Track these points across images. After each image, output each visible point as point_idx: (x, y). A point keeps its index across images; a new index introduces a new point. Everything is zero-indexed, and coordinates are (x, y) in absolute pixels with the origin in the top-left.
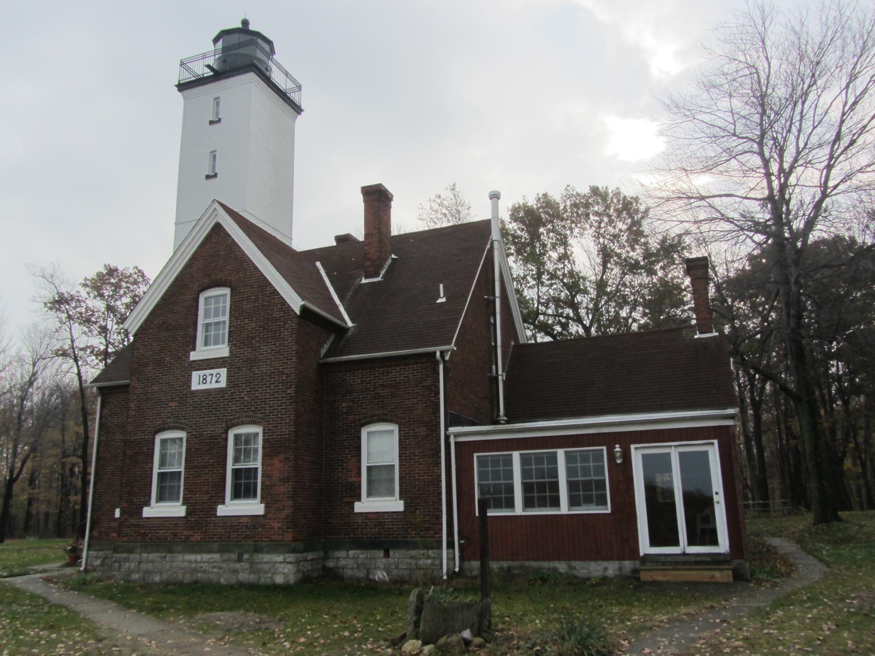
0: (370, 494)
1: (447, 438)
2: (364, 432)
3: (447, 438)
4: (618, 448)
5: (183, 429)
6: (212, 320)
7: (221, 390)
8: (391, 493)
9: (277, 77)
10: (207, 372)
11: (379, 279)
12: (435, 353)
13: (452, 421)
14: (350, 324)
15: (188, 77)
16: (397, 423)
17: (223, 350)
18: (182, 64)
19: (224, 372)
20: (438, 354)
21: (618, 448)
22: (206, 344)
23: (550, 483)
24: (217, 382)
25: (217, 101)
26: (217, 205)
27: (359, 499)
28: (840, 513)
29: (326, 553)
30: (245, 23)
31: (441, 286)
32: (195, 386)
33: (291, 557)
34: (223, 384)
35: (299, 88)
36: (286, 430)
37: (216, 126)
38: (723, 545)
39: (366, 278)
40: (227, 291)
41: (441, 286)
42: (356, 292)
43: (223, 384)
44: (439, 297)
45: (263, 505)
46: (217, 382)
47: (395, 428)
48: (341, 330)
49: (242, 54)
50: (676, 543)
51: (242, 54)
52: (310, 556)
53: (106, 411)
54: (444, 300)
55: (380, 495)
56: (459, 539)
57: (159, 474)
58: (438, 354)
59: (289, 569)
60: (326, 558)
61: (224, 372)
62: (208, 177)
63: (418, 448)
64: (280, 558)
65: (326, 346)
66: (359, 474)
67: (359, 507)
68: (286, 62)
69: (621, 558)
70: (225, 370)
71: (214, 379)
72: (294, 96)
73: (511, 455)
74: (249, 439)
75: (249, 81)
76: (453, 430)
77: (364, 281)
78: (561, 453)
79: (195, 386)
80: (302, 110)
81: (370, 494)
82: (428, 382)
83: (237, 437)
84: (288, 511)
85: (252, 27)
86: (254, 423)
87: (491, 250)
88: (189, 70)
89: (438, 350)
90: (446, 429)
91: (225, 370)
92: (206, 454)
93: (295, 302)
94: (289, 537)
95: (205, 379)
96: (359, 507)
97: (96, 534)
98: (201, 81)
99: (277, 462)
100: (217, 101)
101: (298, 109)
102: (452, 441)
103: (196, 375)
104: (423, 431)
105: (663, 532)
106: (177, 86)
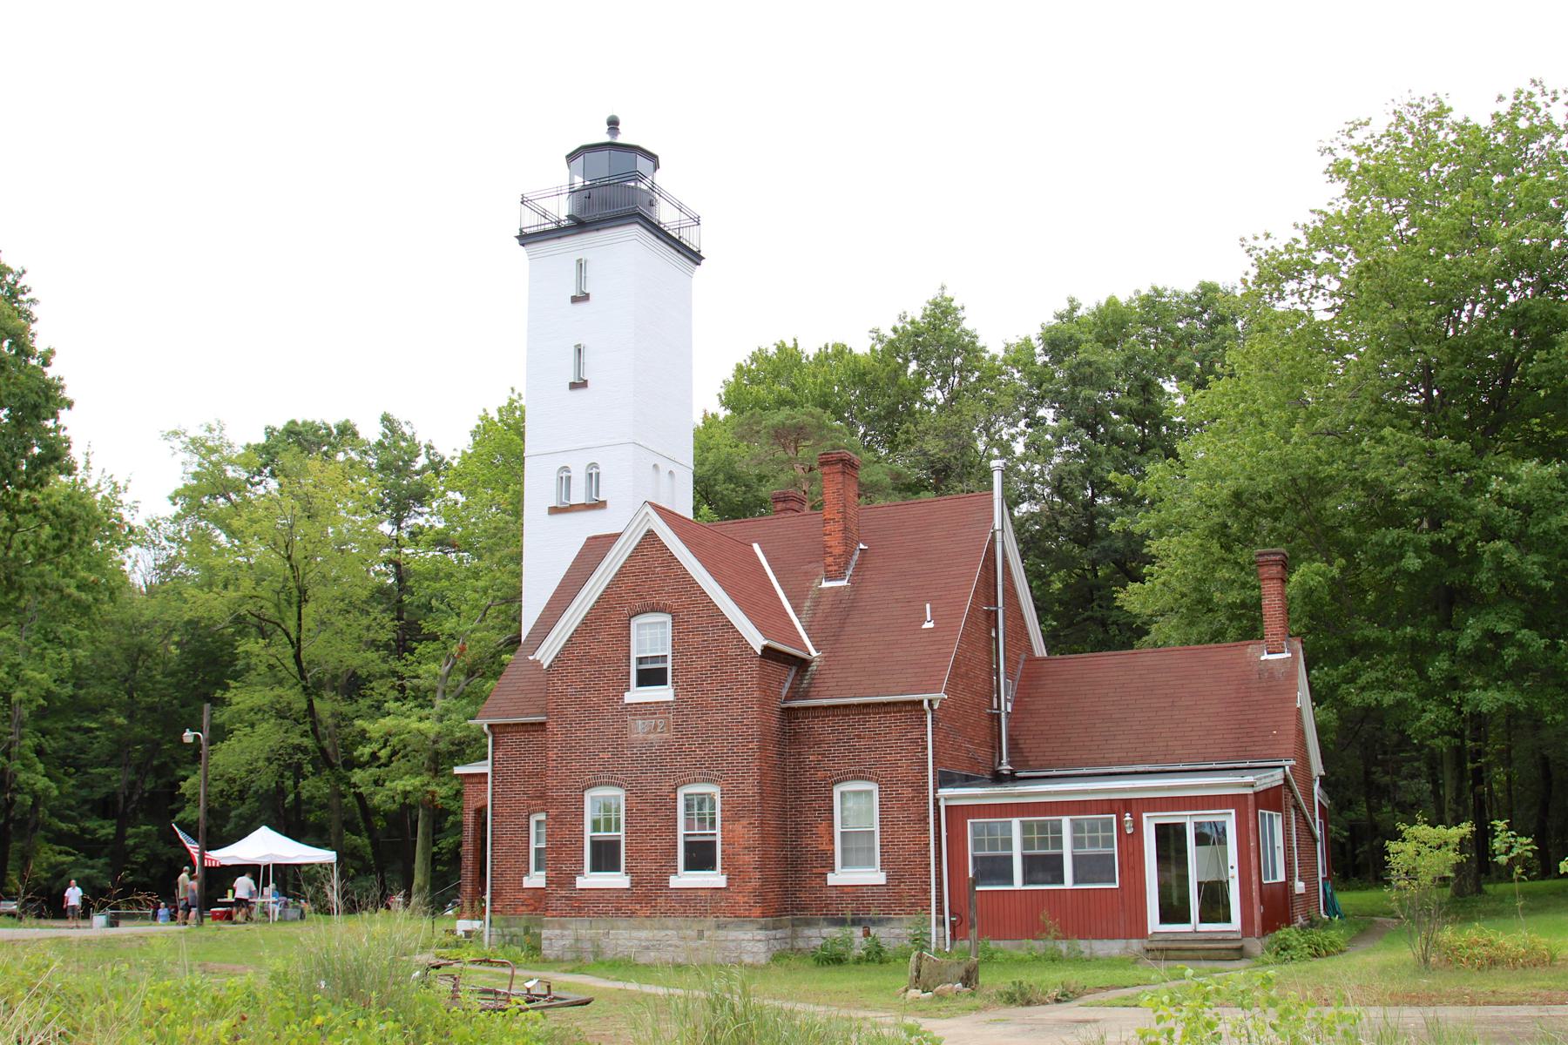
0: (844, 865)
1: (936, 801)
2: (837, 791)
3: (936, 801)
4: (1128, 817)
5: (620, 786)
8: (871, 863)
9: (665, 215)
11: (844, 583)
12: (921, 702)
13: (945, 780)
14: (814, 653)
15: (532, 222)
20: (926, 703)
21: (1128, 817)
25: (581, 265)
26: (649, 509)
28: (1485, 887)
29: (794, 931)
31: (756, 547)
33: (761, 934)
34: (616, 795)
36: (750, 788)
37: (581, 307)
38: (1236, 923)
39: (829, 579)
40: (667, 618)
41: (756, 547)
42: (817, 603)
44: (925, 620)
45: (724, 877)
47: (873, 787)
48: (802, 664)
49: (612, 193)
50: (1187, 920)
51: (612, 193)
52: (779, 934)
53: (499, 754)
54: (931, 625)
55: (857, 864)
56: (951, 915)
57: (686, 835)
58: (926, 703)
59: (762, 947)
60: (794, 937)
63: (904, 809)
64: (749, 936)
65: (787, 685)
66: (832, 842)
67: (832, 879)
68: (676, 187)
69: (1128, 936)
72: (690, 237)
74: (702, 799)
75: (628, 242)
76: (943, 792)
77: (825, 585)
78: (1066, 821)
81: (844, 865)
82: (915, 734)
84: (755, 883)
86: (710, 781)
87: (993, 540)
89: (925, 697)
90: (935, 791)
92: (652, 812)
93: (757, 641)
94: (758, 911)
96: (832, 879)
97: (498, 907)
98: (558, 232)
99: (739, 828)
101: (695, 257)
102: (942, 804)
104: (908, 792)
105: (1173, 911)
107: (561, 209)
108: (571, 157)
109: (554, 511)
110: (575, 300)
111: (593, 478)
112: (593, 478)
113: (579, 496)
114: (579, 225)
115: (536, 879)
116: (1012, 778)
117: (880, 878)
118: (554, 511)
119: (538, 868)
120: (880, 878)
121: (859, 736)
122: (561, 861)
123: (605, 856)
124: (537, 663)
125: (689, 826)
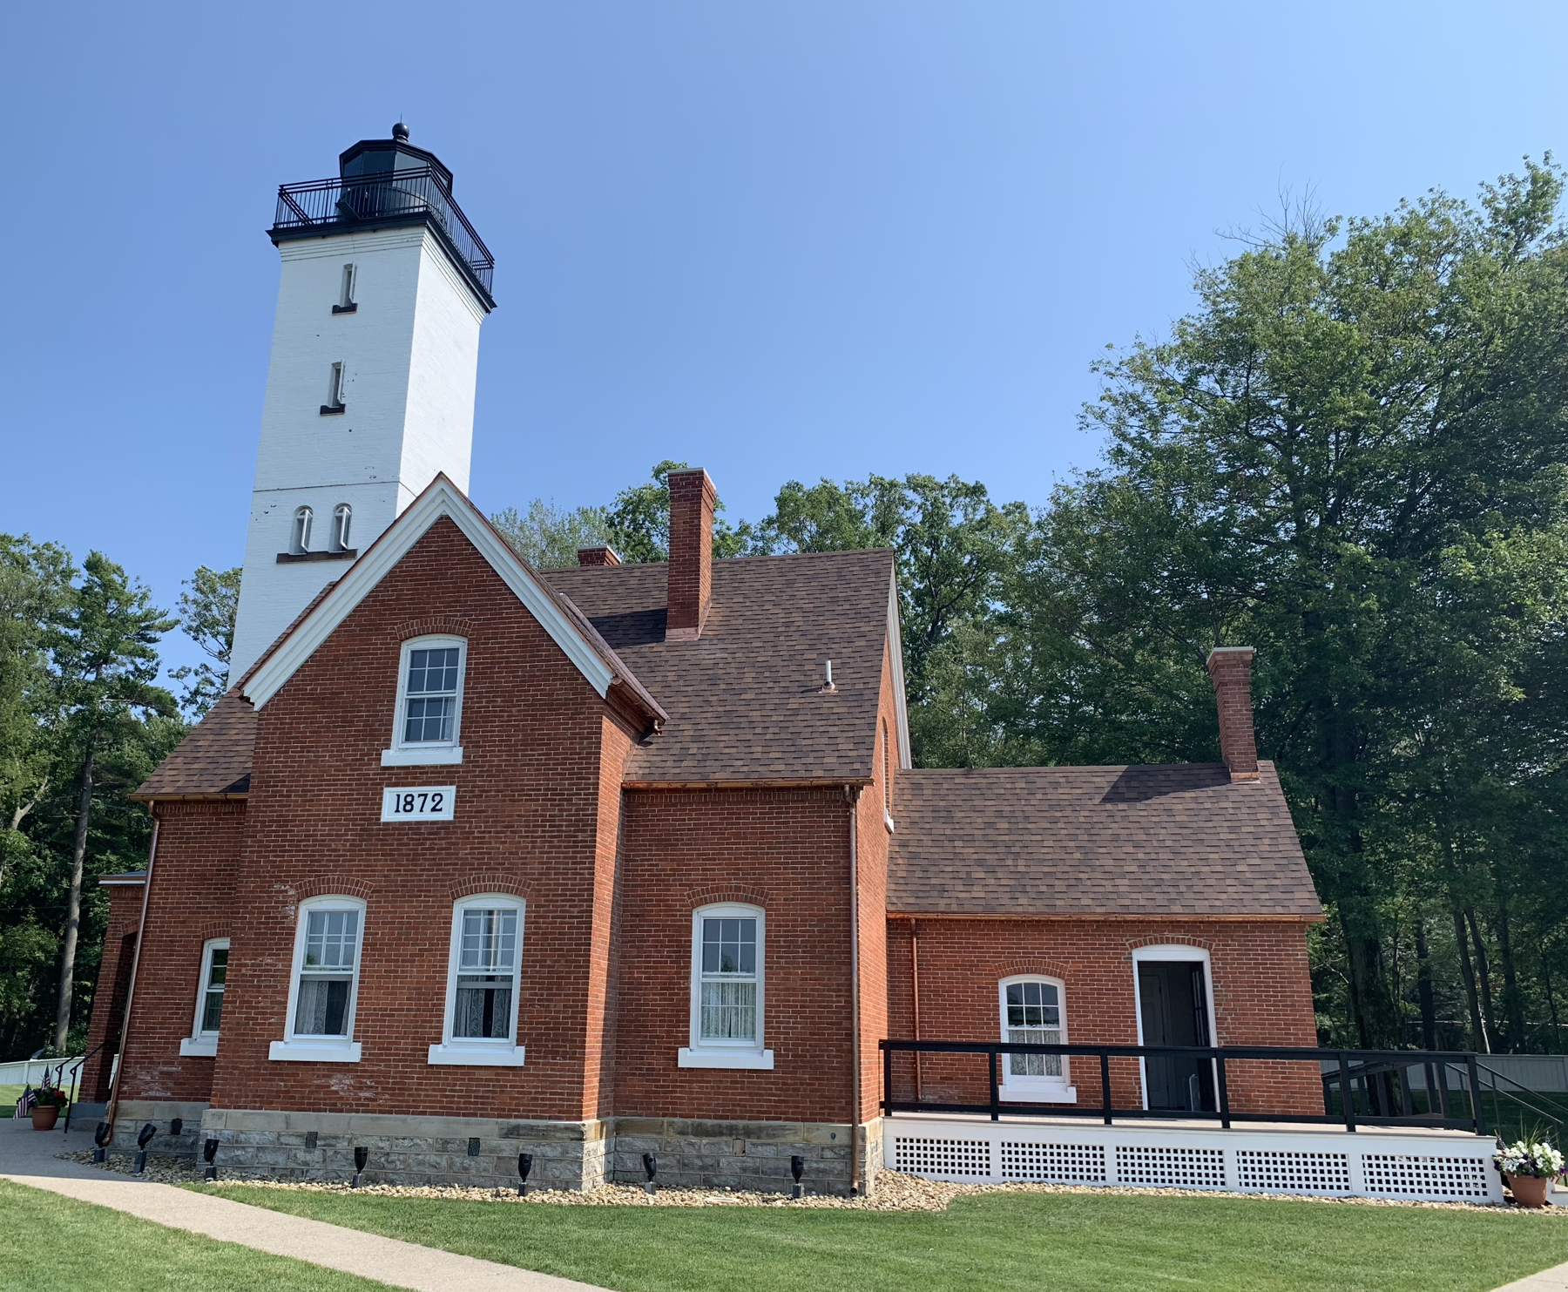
0: (706, 1031)
5: (358, 894)
6: (425, 694)
7: (444, 825)
10: (415, 790)
15: (289, 217)
16: (761, 905)
17: (448, 753)
18: (283, 193)
19: (449, 792)
22: (411, 735)
23: (1020, 1022)
24: (434, 809)
25: (349, 271)
27: (686, 1043)
32: (388, 814)
34: (447, 814)
35: (490, 261)
43: (447, 814)
46: (434, 809)
57: (461, 979)
61: (449, 792)
67: (687, 1058)
70: (453, 788)
71: (429, 804)
79: (388, 814)
80: (276, 243)
83: (314, 916)
85: (412, 141)
88: (294, 207)
91: (453, 788)
95: (410, 803)
96: (687, 1058)
100: (349, 271)
103: (390, 795)
106: (269, 232)
107: (321, 206)
109: (283, 558)
110: (325, 411)
111: (340, 523)
112: (340, 523)
113: (319, 540)
115: (201, 1043)
117: (766, 1061)
118: (283, 558)
119: (208, 1024)
120: (766, 1061)
121: (737, 836)
122: (248, 1022)
123: (485, 1014)
125: (466, 959)
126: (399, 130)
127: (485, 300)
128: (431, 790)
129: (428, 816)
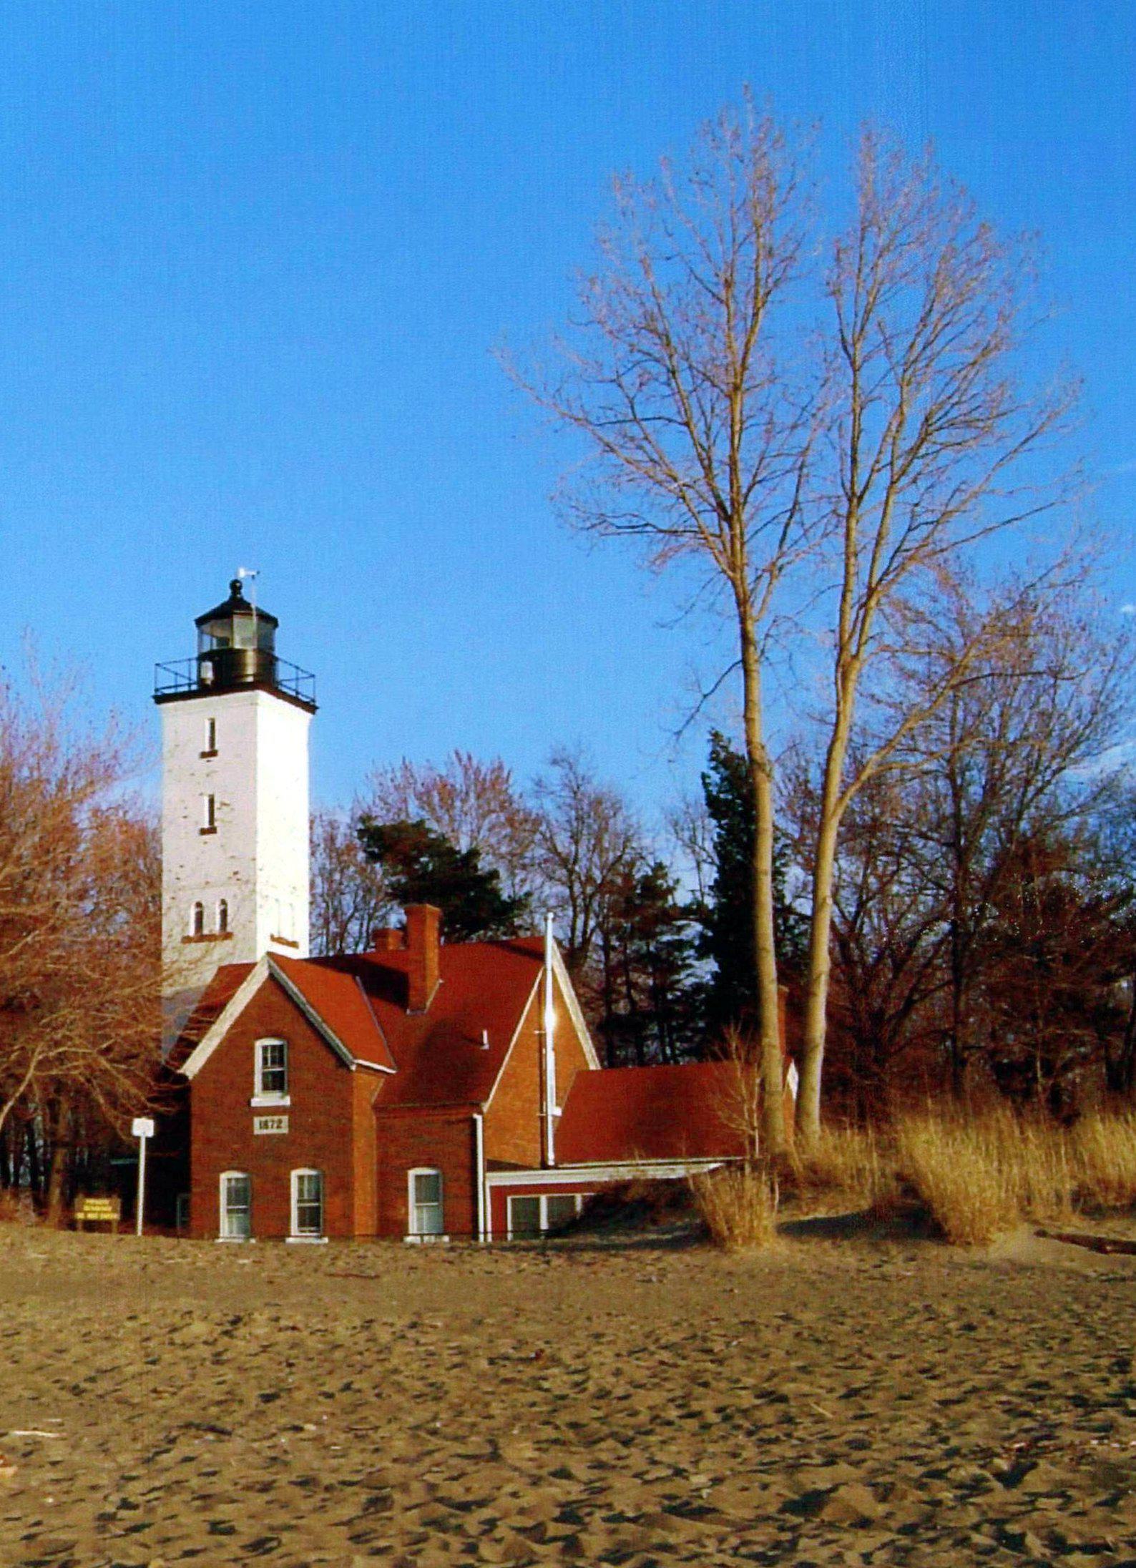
10: (269, 1118)
13: (493, 1166)
19: (285, 1118)
22: (266, 1088)
30: (236, 586)
31: (485, 1034)
32: (257, 1131)
34: (285, 1130)
41: (485, 1034)
43: (285, 1130)
61: (285, 1118)
62: (204, 755)
72: (306, 692)
73: (573, 1198)
79: (257, 1131)
103: (257, 1120)
108: (200, 622)
114: (204, 690)
116: (555, 1167)
124: (183, 1078)
126: (236, 586)
127: (310, 707)
128: (276, 1118)
129: (275, 1131)
